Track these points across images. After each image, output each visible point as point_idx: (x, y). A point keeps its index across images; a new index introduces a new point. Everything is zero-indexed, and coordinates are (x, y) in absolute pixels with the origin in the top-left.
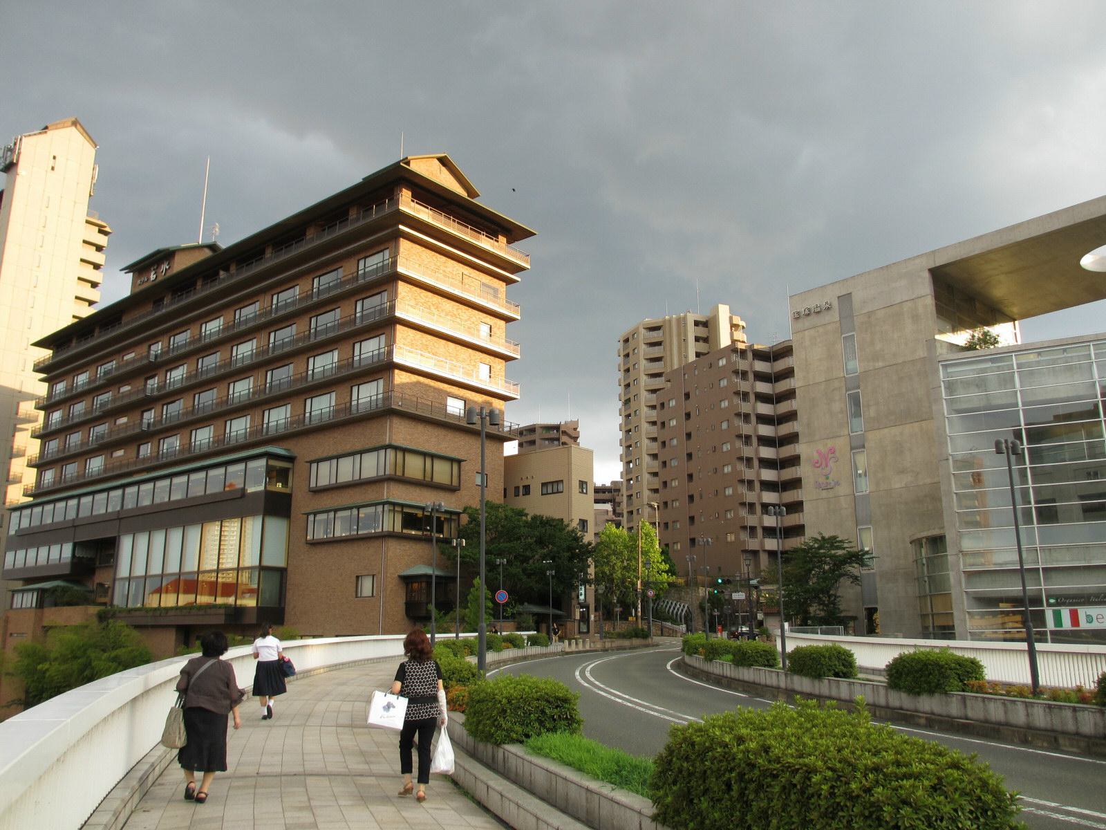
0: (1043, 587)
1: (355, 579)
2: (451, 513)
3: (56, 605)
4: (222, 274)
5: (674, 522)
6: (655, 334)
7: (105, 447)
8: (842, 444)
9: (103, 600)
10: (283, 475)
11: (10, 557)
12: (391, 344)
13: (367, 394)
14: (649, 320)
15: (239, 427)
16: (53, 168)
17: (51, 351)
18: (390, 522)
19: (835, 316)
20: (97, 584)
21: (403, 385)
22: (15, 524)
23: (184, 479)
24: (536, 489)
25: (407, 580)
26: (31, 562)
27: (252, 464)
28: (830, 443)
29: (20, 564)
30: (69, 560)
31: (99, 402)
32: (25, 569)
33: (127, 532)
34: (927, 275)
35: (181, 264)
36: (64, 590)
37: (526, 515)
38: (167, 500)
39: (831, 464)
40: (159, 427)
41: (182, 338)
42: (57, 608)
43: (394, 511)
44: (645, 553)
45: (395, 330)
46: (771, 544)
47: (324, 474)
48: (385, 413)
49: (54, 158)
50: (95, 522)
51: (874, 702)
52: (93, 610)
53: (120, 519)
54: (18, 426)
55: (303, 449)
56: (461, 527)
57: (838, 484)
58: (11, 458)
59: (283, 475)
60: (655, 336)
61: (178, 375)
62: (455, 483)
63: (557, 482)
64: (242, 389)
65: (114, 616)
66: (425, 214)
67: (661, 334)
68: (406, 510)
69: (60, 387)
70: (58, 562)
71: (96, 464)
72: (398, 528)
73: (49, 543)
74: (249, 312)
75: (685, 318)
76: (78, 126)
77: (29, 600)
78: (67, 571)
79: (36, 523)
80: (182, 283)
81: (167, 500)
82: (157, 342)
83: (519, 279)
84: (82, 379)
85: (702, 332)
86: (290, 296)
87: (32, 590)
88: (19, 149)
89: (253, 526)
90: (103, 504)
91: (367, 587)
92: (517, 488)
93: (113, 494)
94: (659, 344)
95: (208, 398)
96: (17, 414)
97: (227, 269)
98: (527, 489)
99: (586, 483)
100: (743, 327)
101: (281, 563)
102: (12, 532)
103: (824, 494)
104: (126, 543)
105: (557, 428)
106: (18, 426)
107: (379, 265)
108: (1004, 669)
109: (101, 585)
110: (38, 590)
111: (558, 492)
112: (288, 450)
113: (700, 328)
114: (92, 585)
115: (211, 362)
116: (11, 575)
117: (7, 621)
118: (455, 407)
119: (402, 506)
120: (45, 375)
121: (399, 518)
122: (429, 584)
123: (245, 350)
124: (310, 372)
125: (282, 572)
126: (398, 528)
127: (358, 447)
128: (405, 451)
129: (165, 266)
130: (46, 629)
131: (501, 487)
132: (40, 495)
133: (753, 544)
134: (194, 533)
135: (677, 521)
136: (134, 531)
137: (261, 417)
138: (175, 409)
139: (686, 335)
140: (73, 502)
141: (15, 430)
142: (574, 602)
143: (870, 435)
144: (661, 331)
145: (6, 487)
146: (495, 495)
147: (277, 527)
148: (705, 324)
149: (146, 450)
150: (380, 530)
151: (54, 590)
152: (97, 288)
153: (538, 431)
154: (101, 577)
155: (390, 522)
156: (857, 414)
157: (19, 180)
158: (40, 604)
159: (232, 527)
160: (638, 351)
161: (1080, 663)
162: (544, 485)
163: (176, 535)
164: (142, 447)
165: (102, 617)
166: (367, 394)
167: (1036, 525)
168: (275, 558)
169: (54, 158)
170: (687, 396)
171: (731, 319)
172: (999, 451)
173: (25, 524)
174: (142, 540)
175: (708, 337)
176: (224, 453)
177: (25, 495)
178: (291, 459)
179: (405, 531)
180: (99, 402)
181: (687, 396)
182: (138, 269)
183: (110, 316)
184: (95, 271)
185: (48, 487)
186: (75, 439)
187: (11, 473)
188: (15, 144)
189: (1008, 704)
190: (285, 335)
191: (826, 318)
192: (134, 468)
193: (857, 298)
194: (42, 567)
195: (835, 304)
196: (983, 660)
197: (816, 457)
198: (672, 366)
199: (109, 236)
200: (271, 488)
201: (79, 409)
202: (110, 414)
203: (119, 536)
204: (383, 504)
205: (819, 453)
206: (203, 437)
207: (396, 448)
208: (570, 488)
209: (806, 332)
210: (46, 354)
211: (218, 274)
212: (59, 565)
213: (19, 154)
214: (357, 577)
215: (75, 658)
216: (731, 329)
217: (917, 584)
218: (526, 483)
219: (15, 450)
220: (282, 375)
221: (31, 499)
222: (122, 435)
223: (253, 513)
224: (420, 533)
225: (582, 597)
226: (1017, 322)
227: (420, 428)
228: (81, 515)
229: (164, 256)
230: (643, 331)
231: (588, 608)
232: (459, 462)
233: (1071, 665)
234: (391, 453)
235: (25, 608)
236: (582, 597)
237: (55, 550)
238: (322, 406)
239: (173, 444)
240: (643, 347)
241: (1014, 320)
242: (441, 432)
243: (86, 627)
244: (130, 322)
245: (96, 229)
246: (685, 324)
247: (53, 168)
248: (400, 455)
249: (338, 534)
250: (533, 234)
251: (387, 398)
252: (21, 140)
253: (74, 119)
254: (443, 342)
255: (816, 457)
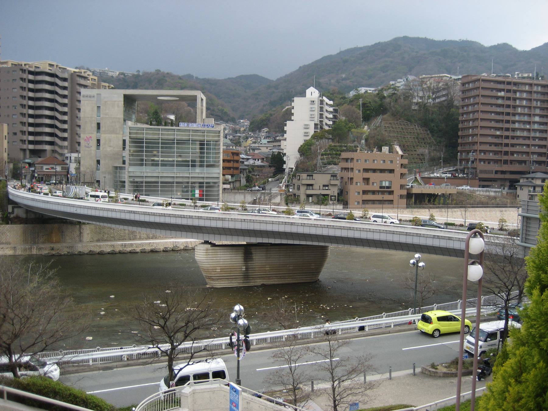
0: (160, 136)
19: (95, 99)
28: (90, 135)
34: (123, 96)
39: (90, 141)
46: (31, 147)
56: (468, 284)
57: (91, 147)
103: (87, 149)
108: (490, 144)
133: (25, 147)
191: (92, 99)
195: (96, 95)
197: (86, 138)
205: (87, 137)
217: (235, 284)
255: (86, 138)
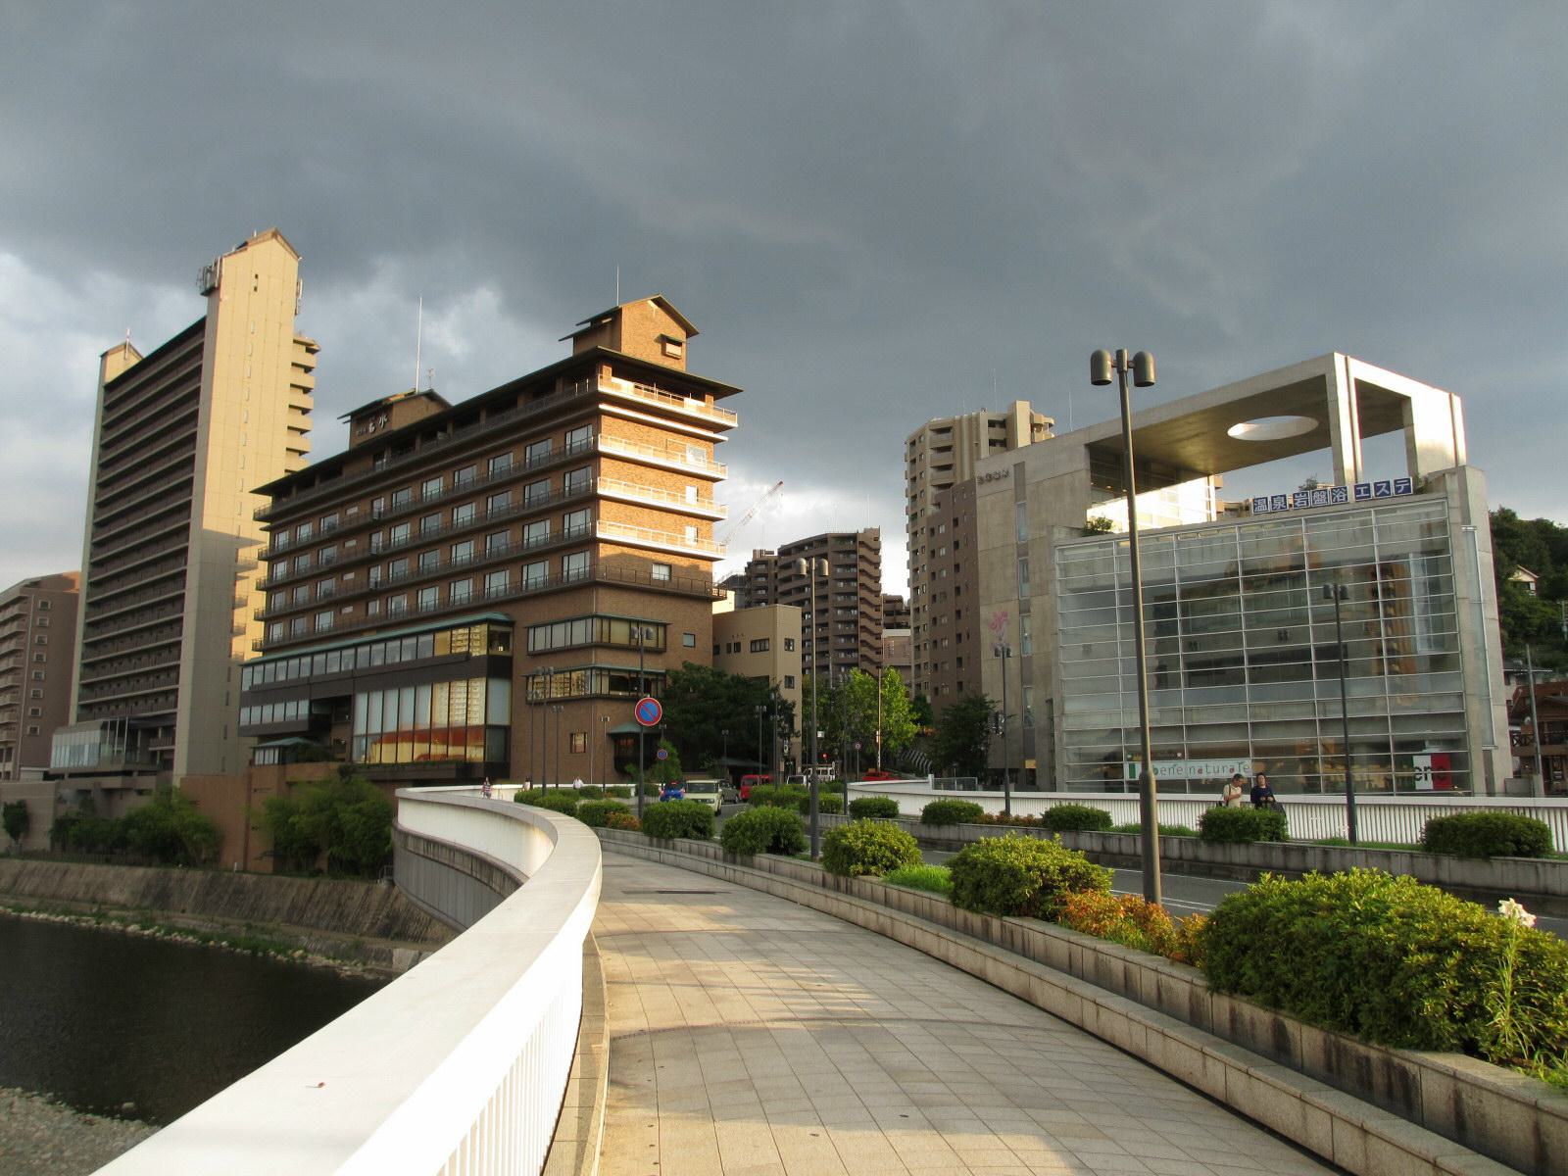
1: (568, 736)
2: (657, 674)
3: (297, 761)
4: (440, 435)
5: (943, 663)
6: (944, 436)
7: (333, 603)
8: (1012, 608)
9: (340, 756)
10: (504, 639)
11: (245, 712)
12: (595, 517)
13: (576, 565)
14: (938, 419)
15: (463, 590)
16: (256, 289)
17: (270, 498)
18: (600, 685)
20: (335, 740)
21: (607, 558)
22: (248, 680)
23: (413, 641)
24: (746, 647)
25: (615, 738)
26: (267, 719)
27: (477, 630)
29: (256, 720)
30: (306, 718)
31: (324, 557)
32: (261, 725)
33: (362, 691)
34: (1083, 450)
35: (400, 420)
36: (305, 747)
37: (725, 675)
38: (397, 660)
39: (1004, 626)
40: (389, 516)
41: (404, 496)
42: (299, 765)
43: (601, 675)
44: (888, 702)
45: (598, 505)
47: (540, 640)
48: (590, 584)
49: (256, 276)
50: (329, 680)
51: (1249, 861)
52: (334, 766)
53: (354, 678)
54: (239, 574)
55: (523, 614)
58: (234, 609)
59: (504, 639)
60: (944, 440)
61: (401, 533)
62: (661, 646)
63: (765, 640)
64: (464, 552)
65: (354, 771)
66: (625, 389)
67: (951, 438)
68: (612, 674)
69: (283, 538)
70: (294, 718)
71: (325, 620)
72: (605, 690)
73: (285, 700)
74: (468, 475)
75: (977, 418)
76: (279, 237)
77: (271, 757)
78: (305, 728)
79: (269, 679)
80: (402, 441)
81: (397, 660)
82: (380, 498)
83: (726, 439)
84: (305, 531)
85: (998, 433)
86: (504, 463)
87: (274, 747)
88: (220, 272)
89: (479, 687)
90: (336, 663)
91: (579, 741)
92: (729, 645)
93: (346, 653)
94: (948, 449)
95: (432, 559)
96: (236, 561)
97: (444, 430)
98: (738, 647)
99: (793, 640)
100: (1050, 425)
101: (505, 722)
102: (246, 688)
104: (361, 702)
105: (853, 537)
106: (239, 574)
107: (583, 442)
109: (338, 741)
110: (279, 747)
111: (765, 650)
112: (506, 614)
113: (997, 429)
114: (330, 741)
115: (433, 523)
116: (245, 731)
117: (250, 777)
118: (660, 573)
119: (609, 670)
120: (269, 524)
121: (606, 682)
122: (637, 742)
123: (465, 514)
124: (568, 447)
125: (506, 730)
126: (605, 690)
127: (569, 615)
128: (610, 619)
129: (383, 419)
130: (290, 784)
131: (710, 645)
132: (267, 647)
134: (425, 693)
135: (946, 662)
136: (369, 690)
137: (482, 581)
138: (401, 568)
139: (978, 438)
140: (307, 660)
141: (236, 579)
142: (778, 755)
143: (1035, 601)
144: (950, 434)
145: (231, 640)
146: (703, 658)
147: (500, 688)
148: (1003, 424)
149: (375, 607)
150: (589, 692)
151: (294, 747)
152: (309, 394)
153: (831, 542)
154: (338, 733)
155: (600, 685)
156: (1026, 580)
157: (222, 306)
158: (283, 761)
159: (460, 687)
160: (925, 458)
161: (1368, 812)
162: (752, 642)
163: (408, 695)
164: (372, 570)
165: (344, 772)
166: (576, 565)
167: (1183, 688)
168: (500, 718)
169: (256, 276)
170: (956, 522)
171: (1031, 417)
172: (997, 655)
173: (258, 680)
174: (377, 698)
175: (1005, 439)
176: (448, 612)
177: (255, 649)
178: (511, 624)
179: (612, 693)
180: (324, 557)
181: (956, 522)
182: (360, 417)
183: (330, 469)
184: (306, 375)
185: (278, 642)
186: (302, 593)
187: (235, 624)
188: (216, 264)
189: (1539, 865)
190: (502, 502)
192: (364, 627)
193: (1028, 468)
194: (279, 724)
195: (1012, 471)
196: (981, 803)
198: (962, 477)
199: (316, 354)
200: (492, 652)
201: (305, 563)
202: (337, 570)
203: (354, 695)
204: (592, 669)
205: (995, 615)
206: (429, 597)
207: (602, 618)
208: (775, 645)
209: (988, 498)
210: (266, 501)
211: (436, 435)
212: (297, 721)
213: (220, 277)
214: (572, 735)
215: (322, 810)
216: (1032, 430)
218: (736, 640)
219: (237, 600)
220: (501, 541)
221: (261, 654)
222: (351, 593)
223: (478, 676)
224: (627, 694)
225: (786, 751)
226: (1212, 478)
227: (626, 596)
228: (315, 673)
229: (379, 409)
230: (929, 434)
231: (794, 760)
232: (665, 626)
233: (1368, 815)
234: (597, 622)
235: (269, 765)
236: (786, 751)
237: (291, 708)
238: (537, 574)
239: (400, 603)
240: (930, 453)
241: (1208, 475)
242: (646, 599)
243: (330, 782)
244: (350, 475)
245: (304, 348)
246: (978, 425)
247: (256, 289)
248: (606, 624)
249: (553, 695)
250: (735, 391)
251: (593, 572)
252: (221, 261)
253: (273, 230)
254: (647, 510)
